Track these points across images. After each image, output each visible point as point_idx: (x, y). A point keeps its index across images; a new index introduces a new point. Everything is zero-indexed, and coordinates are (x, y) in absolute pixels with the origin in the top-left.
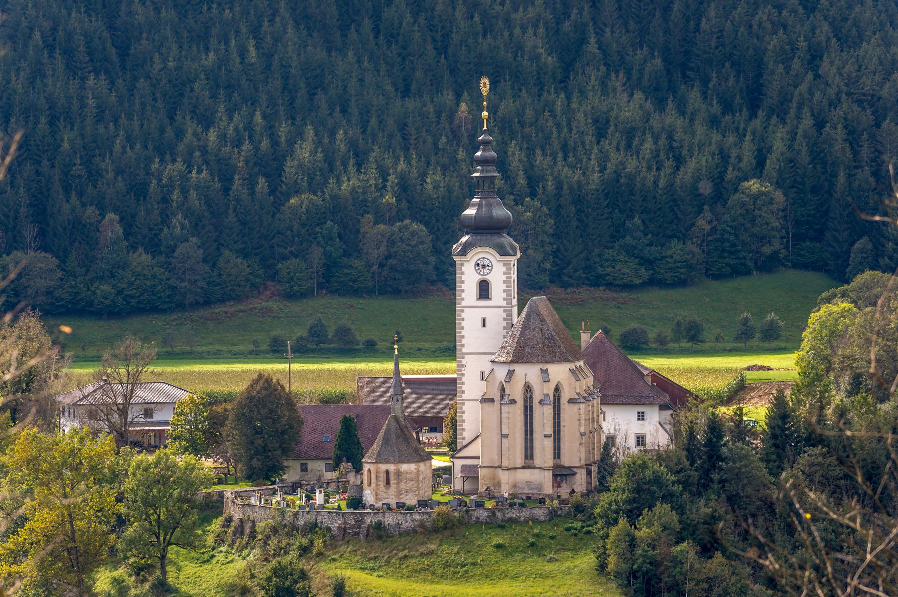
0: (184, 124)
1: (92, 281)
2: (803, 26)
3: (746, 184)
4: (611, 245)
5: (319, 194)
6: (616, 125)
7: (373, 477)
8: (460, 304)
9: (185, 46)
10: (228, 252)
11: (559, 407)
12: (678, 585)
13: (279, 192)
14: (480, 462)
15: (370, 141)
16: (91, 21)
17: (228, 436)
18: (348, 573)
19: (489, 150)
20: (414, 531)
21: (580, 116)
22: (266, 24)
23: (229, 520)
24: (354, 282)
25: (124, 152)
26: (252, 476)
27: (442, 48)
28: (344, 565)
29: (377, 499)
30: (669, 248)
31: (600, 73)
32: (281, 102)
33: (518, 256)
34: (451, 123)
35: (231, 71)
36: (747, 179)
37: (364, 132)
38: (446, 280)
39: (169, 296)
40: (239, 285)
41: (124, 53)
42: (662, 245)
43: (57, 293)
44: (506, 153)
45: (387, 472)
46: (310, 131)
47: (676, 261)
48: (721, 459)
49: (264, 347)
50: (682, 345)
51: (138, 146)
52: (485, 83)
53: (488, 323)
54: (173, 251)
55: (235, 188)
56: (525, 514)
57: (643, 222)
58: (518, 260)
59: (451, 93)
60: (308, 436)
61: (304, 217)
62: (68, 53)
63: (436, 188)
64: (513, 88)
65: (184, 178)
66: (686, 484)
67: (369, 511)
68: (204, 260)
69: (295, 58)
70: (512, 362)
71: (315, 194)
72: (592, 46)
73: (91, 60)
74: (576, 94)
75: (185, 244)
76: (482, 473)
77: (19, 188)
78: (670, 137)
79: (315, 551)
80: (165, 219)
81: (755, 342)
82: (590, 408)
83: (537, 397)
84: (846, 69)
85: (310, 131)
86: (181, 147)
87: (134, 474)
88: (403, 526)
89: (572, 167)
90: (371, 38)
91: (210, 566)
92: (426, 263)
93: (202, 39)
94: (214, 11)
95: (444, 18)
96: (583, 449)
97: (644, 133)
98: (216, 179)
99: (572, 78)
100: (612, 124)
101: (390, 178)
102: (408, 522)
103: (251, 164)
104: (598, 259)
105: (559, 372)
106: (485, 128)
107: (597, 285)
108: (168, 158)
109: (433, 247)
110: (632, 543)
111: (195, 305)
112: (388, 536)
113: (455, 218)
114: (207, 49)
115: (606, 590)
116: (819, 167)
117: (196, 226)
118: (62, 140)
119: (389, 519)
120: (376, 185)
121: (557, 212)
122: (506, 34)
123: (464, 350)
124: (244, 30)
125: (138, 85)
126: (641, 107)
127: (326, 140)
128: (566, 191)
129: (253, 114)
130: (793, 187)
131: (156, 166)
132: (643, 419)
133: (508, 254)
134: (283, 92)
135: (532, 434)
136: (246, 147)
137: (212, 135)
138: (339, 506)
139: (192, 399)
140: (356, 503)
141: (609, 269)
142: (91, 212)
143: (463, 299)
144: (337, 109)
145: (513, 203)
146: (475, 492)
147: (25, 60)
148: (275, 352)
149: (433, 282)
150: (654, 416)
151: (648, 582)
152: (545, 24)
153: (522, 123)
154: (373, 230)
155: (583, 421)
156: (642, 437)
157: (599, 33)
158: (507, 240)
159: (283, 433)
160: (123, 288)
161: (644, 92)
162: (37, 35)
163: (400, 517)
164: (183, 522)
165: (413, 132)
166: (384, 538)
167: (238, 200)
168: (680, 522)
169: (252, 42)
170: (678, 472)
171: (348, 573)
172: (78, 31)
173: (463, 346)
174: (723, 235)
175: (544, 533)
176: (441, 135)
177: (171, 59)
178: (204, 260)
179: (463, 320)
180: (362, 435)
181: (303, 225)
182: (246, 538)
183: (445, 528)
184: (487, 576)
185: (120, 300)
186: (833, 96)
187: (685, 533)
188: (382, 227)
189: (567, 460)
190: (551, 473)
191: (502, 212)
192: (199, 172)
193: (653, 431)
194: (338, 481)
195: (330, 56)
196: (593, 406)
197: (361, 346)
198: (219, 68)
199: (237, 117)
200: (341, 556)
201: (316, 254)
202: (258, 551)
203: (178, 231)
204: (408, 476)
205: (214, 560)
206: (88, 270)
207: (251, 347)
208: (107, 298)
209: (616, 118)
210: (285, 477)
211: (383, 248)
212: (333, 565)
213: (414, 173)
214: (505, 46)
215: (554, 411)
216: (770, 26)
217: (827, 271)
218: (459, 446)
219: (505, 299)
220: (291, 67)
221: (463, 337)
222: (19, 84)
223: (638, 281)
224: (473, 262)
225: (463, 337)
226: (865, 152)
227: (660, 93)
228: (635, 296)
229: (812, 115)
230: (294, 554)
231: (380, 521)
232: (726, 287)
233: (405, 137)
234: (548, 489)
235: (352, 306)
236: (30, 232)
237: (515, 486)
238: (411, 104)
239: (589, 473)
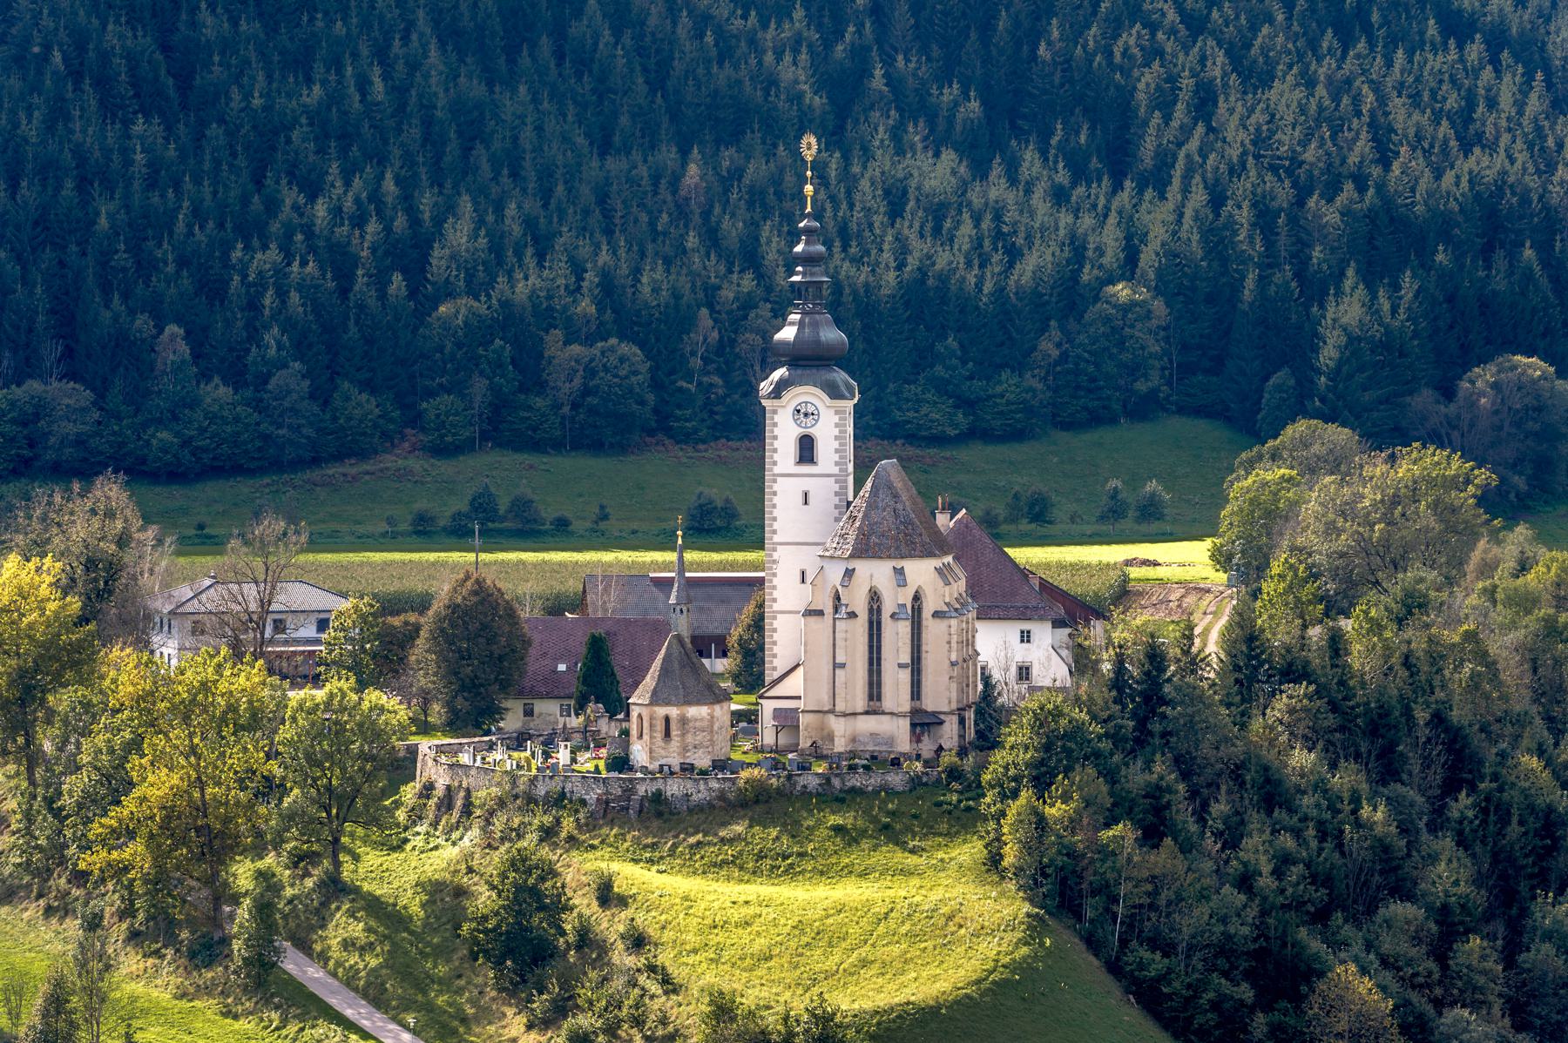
0: (279, 191)
1: (144, 426)
2: (1187, 54)
3: (1111, 289)
4: (912, 377)
5: (483, 299)
6: (918, 200)
7: (646, 724)
9: (277, 75)
10: (346, 385)
11: (919, 623)
12: (1107, 886)
13: (424, 296)
14: (801, 704)
15: (555, 219)
16: (135, 37)
17: (419, 662)
18: (615, 866)
19: (814, 243)
20: (711, 806)
21: (865, 184)
22: (397, 43)
23: (429, 787)
24: (534, 430)
25: (191, 234)
26: (455, 724)
27: (657, 82)
28: (607, 856)
30: (999, 382)
31: (891, 122)
32: (421, 160)
34: (674, 193)
35: (346, 113)
36: (1112, 281)
37: (545, 206)
38: (671, 428)
39: (260, 449)
40: (364, 434)
41: (184, 81)
42: (988, 379)
43: (94, 443)
44: (757, 240)
45: (667, 719)
46: (466, 205)
47: (1009, 403)
48: (1164, 701)
49: (403, 527)
50: (1021, 527)
51: (211, 224)
52: (809, 144)
53: (811, 499)
54: (266, 382)
55: (357, 288)
56: (872, 781)
57: (962, 346)
59: (674, 149)
60: (534, 664)
61: (460, 333)
62: (103, 83)
63: (656, 290)
64: (764, 143)
65: (280, 273)
66: (1115, 737)
67: (639, 775)
68: (312, 396)
69: (441, 95)
70: (852, 556)
71: (477, 299)
72: (878, 81)
73: (137, 95)
74: (856, 152)
75: (284, 372)
76: (804, 720)
77: (34, 286)
78: (998, 218)
79: (563, 835)
80: (254, 334)
81: (1127, 524)
83: (888, 608)
84: (1253, 120)
85: (466, 205)
86: (275, 227)
87: (294, 719)
88: (695, 797)
89: (857, 261)
90: (552, 65)
91: (403, 856)
92: (642, 403)
93: (300, 64)
94: (320, 24)
95: (660, 36)
96: (954, 686)
97: (960, 213)
98: (329, 275)
99: (849, 127)
100: (912, 197)
101: (587, 276)
102: (701, 792)
103: (380, 253)
104: (893, 399)
105: (921, 572)
106: (809, 209)
107: (892, 438)
108: (256, 242)
109: (652, 378)
110: (1041, 823)
111: (298, 464)
112: (671, 813)
113: (685, 337)
114: (309, 81)
115: (1002, 894)
116: (1215, 264)
117: (300, 347)
118: (98, 214)
119: (674, 788)
120: (567, 287)
122: (753, 61)
123: (776, 607)
124: (365, 51)
125: (208, 133)
126: (954, 173)
127: (490, 218)
128: (847, 298)
129: (380, 177)
130: (1178, 294)
131: (239, 254)
133: (842, 397)
134: (423, 146)
135: (879, 664)
136: (373, 227)
137: (321, 210)
138: (597, 767)
139: (356, 608)
140: (621, 763)
141: (911, 414)
142: (142, 323)
143: (775, 463)
144: (505, 172)
145: (770, 314)
146: (794, 748)
147: (39, 95)
148: (418, 533)
149: (651, 433)
151: (1064, 881)
152: (810, 46)
153: (780, 195)
154: (563, 353)
155: (954, 645)
157: (888, 62)
158: (841, 376)
159: (501, 659)
160: (191, 438)
161: (956, 150)
162: (57, 57)
163: (689, 784)
164: (366, 789)
165: (619, 206)
166: (666, 816)
167: (361, 307)
168: (1111, 794)
169: (377, 71)
170: (1105, 721)
171: (615, 866)
172: (118, 50)
173: (774, 532)
174: (1077, 364)
175: (903, 809)
176: (660, 212)
177: (256, 94)
178: (312, 396)
179: (775, 494)
180: (620, 661)
181: (459, 345)
182: (456, 814)
183: (757, 802)
184: (822, 873)
185: (186, 455)
186: (1235, 160)
187: (1117, 811)
188: (576, 349)
191: (832, 335)
192: (304, 263)
193: (1043, 659)
194: (584, 731)
195: (492, 92)
197: (547, 527)
198: (329, 108)
199: (357, 182)
200: (602, 842)
201: (479, 387)
202: (474, 833)
203: (272, 352)
205: (408, 847)
206: (138, 410)
207: (383, 527)
208: (167, 452)
209: (918, 188)
210: (501, 724)
211: (577, 381)
212: (590, 855)
213: (624, 269)
214: (751, 79)
216: (1139, 55)
217: (1229, 420)
218: (768, 680)
219: (837, 464)
220: (435, 107)
221: (775, 519)
222: (31, 129)
223: (953, 432)
224: (790, 409)
225: (775, 519)
226: (1283, 241)
227: (980, 151)
228: (948, 454)
229: (1206, 188)
230: (530, 840)
231: (659, 790)
232: (1080, 442)
233: (607, 215)
234: (904, 745)
235: (531, 467)
236: (51, 351)
237: (854, 740)
238: (615, 165)
239: (962, 721)
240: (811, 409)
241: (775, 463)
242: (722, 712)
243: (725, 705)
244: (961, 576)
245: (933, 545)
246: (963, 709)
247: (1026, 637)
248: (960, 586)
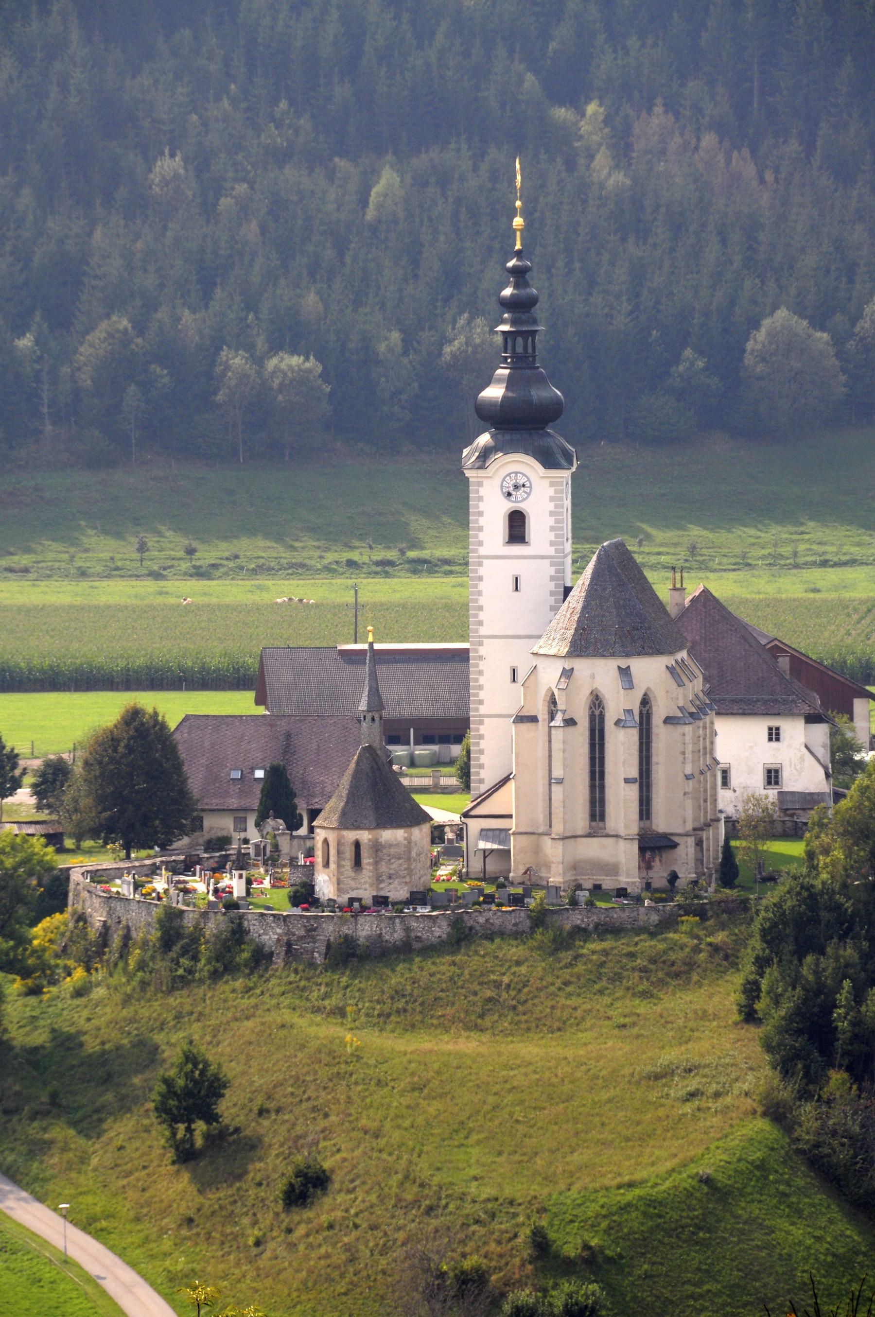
7: (333, 851)
8: (476, 551)
10: (137, 1080)
29: (340, 891)
33: (574, 469)
45: (357, 845)
53: (522, 584)
58: (573, 474)
82: (701, 732)
96: (689, 803)
105: (650, 670)
106: (518, 246)
123: (483, 710)
132: (778, 740)
140: (304, 895)
155: (689, 755)
156: (777, 771)
189: (661, 824)
190: (635, 846)
196: (705, 728)
215: (641, 738)
219: (552, 544)
221: (481, 608)
225: (481, 608)
234: (629, 877)
240: (521, 480)
241: (480, 543)
244: (697, 672)
247: (774, 735)
248: (697, 685)
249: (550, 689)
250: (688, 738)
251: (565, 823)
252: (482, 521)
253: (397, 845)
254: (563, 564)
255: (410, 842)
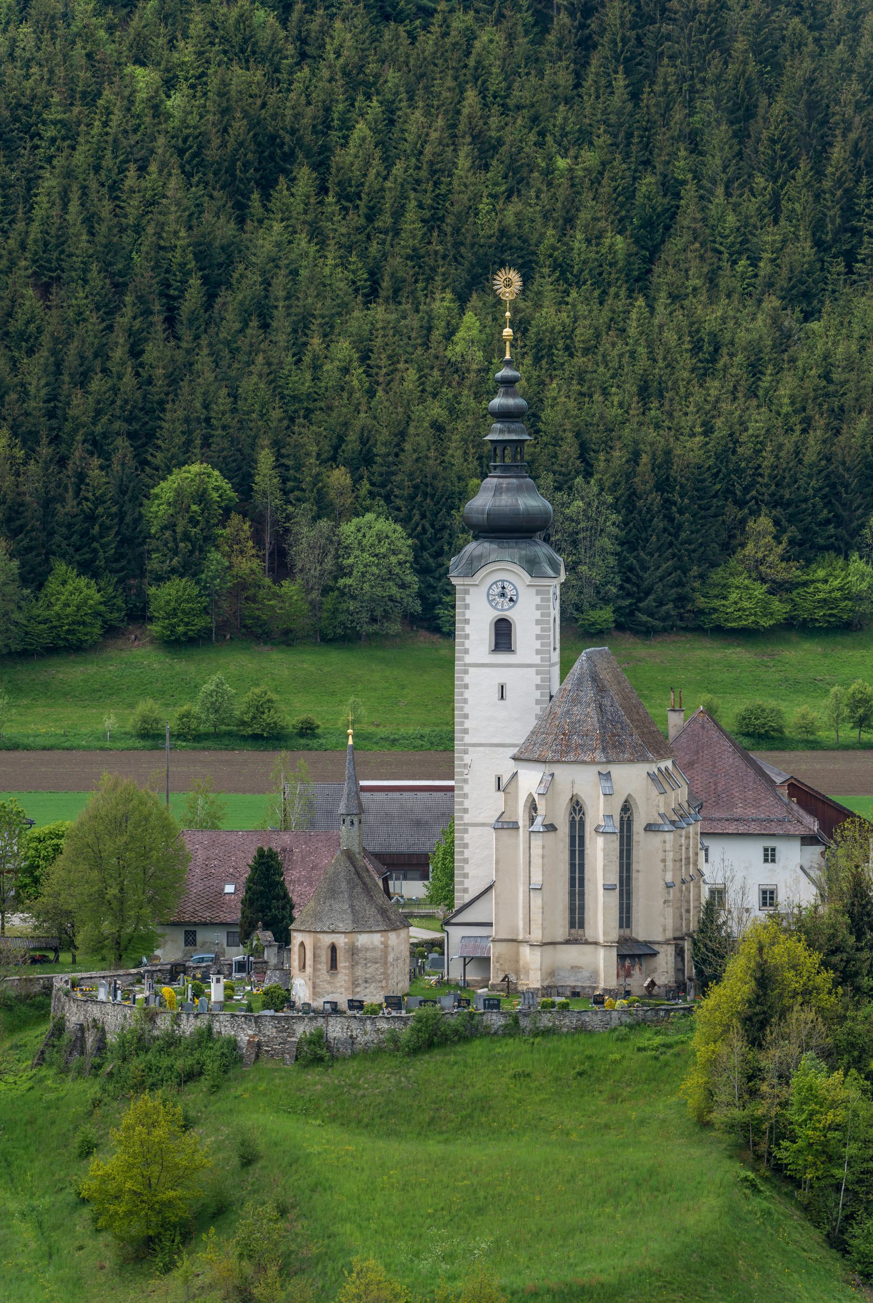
14: (492, 932)
29: (315, 994)
40: (84, 623)
45: (333, 948)
53: (508, 693)
59: (449, 295)
96: (670, 911)
102: (367, 1034)
105: (632, 778)
106: (508, 357)
119: (336, 1030)
121: (628, 503)
132: (773, 861)
143: (466, 651)
150: (792, 855)
155: (670, 864)
156: (772, 893)
163: (355, 1024)
189: (641, 931)
204: (369, 955)
215: (621, 844)
219: (538, 652)
223: (766, 622)
237: (552, 974)
238: (380, 312)
239: (680, 953)
241: (466, 651)
242: (399, 942)
243: (403, 933)
244: (683, 783)
245: (653, 744)
246: (682, 939)
247: (770, 856)
248: (682, 794)
249: (530, 795)
250: (668, 846)
251: (543, 929)
252: (468, 629)
253: (374, 949)
254: (549, 672)
255: (386, 946)
